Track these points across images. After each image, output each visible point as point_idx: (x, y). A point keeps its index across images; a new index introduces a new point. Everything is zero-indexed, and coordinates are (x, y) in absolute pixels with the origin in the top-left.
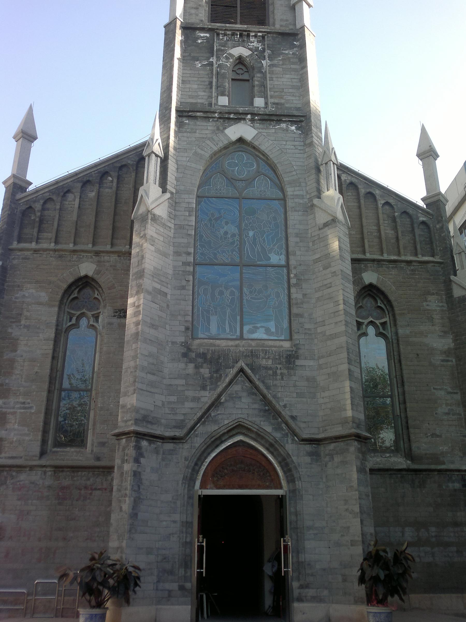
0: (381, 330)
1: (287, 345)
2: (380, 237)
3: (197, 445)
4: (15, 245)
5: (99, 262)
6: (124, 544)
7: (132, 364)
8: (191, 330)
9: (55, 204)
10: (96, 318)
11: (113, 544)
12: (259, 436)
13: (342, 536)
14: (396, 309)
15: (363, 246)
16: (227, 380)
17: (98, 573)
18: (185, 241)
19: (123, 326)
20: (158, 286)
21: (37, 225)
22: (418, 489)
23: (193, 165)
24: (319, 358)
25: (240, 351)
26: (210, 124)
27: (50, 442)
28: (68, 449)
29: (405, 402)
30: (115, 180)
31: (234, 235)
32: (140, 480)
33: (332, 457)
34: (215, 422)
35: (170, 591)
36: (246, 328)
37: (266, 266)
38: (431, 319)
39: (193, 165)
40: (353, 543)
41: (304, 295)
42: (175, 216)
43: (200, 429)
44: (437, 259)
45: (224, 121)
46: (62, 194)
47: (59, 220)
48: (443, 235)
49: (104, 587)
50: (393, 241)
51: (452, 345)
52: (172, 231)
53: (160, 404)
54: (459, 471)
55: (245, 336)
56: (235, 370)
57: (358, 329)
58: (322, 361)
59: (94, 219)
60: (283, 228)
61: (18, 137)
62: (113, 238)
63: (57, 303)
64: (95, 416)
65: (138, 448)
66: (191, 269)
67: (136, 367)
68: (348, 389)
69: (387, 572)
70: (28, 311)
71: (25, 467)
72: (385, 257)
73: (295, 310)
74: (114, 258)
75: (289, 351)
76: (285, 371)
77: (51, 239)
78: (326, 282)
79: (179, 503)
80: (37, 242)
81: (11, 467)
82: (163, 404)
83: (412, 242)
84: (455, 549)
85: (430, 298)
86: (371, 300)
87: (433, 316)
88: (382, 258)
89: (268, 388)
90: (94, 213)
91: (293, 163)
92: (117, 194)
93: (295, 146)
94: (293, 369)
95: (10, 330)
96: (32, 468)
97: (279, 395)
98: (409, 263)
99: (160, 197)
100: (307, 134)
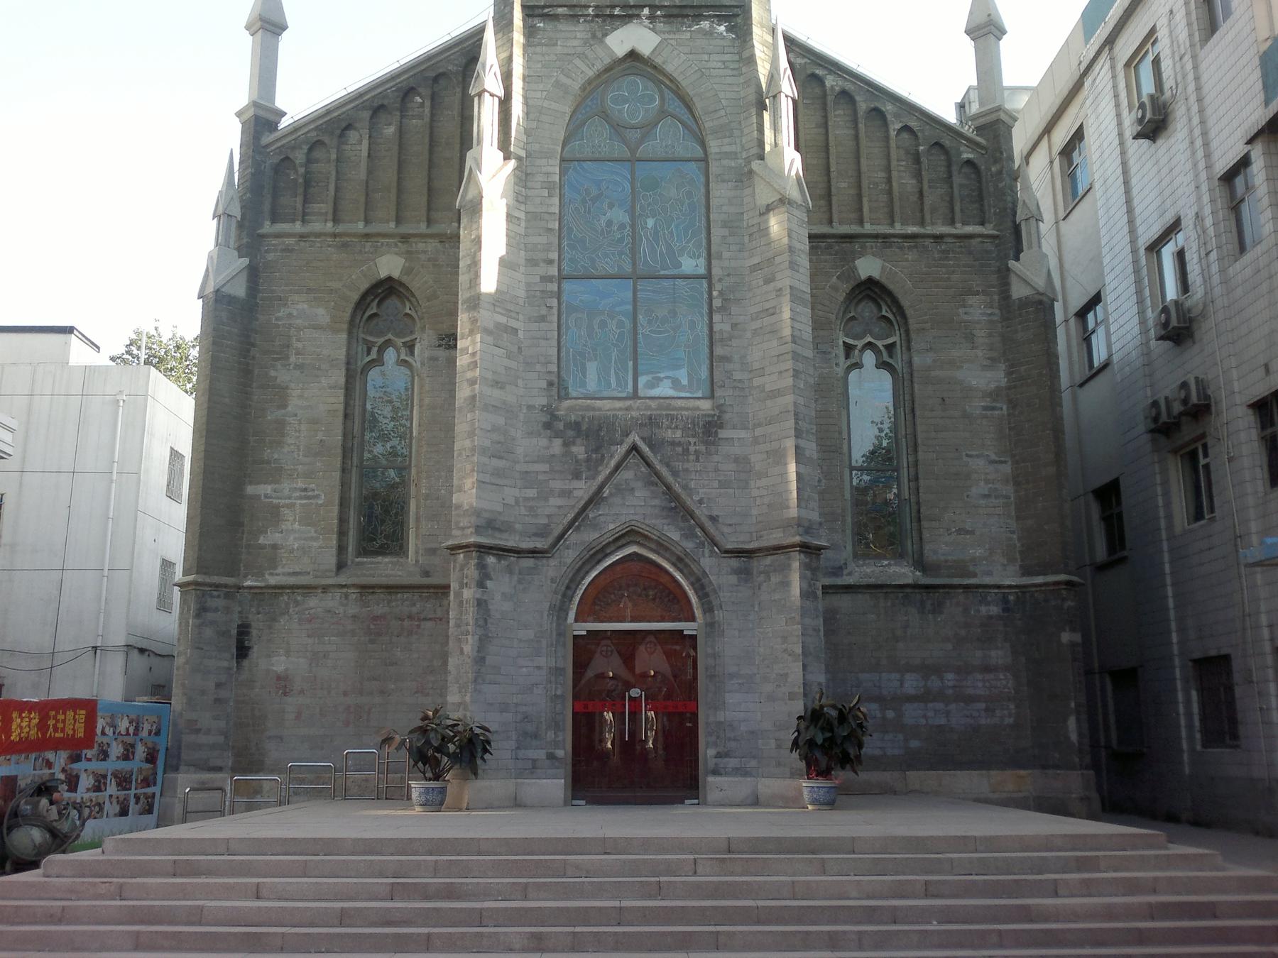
0: (886, 358)
1: (706, 405)
2: (890, 192)
3: (569, 561)
4: (267, 228)
5: (408, 252)
6: (468, 698)
7: (467, 443)
8: (558, 387)
9: (328, 152)
10: (410, 347)
11: (453, 698)
12: (662, 547)
13: (778, 686)
14: (911, 321)
15: (860, 210)
16: (613, 463)
17: (432, 735)
18: (543, 240)
19: (452, 362)
20: (503, 320)
21: (301, 190)
22: (930, 616)
23: (554, 106)
24: (755, 426)
25: (632, 418)
26: (581, 27)
27: (350, 549)
28: (380, 559)
29: (917, 479)
30: (428, 103)
31: (622, 226)
32: (488, 610)
33: (767, 574)
34: (595, 526)
35: (534, 761)
36: (642, 380)
37: (674, 277)
38: (970, 338)
39: (554, 106)
40: (792, 696)
41: (734, 326)
42: (527, 197)
43: (572, 537)
44: (988, 230)
45: (604, 21)
46: (338, 132)
47: (338, 179)
48: (1001, 185)
49: (443, 753)
50: (914, 198)
51: (1004, 382)
52: (523, 224)
53: (512, 502)
54: (999, 587)
55: (641, 393)
56: (625, 447)
57: (847, 356)
58: (758, 432)
59: (395, 178)
60: (703, 210)
61: (255, 28)
62: (429, 209)
63: (345, 326)
64: (418, 507)
65: (482, 566)
66: (555, 287)
67: (473, 449)
68: (793, 476)
69: (828, 735)
70: (298, 340)
71: (315, 587)
72: (898, 229)
73: (718, 351)
74: (432, 245)
75: (709, 416)
76: (703, 448)
77: (326, 213)
78: (767, 305)
79: (544, 642)
80: (303, 221)
81: (292, 587)
82: (517, 502)
83: (947, 199)
84: (983, 705)
85: (972, 300)
86: (871, 305)
87: (975, 332)
88: (892, 231)
89: (675, 474)
90: (396, 167)
91: (721, 95)
92: (431, 128)
93: (724, 62)
94: (713, 444)
95: (273, 373)
96: (325, 589)
97: (692, 485)
98: (938, 238)
99: (501, 169)
100: (745, 41)
